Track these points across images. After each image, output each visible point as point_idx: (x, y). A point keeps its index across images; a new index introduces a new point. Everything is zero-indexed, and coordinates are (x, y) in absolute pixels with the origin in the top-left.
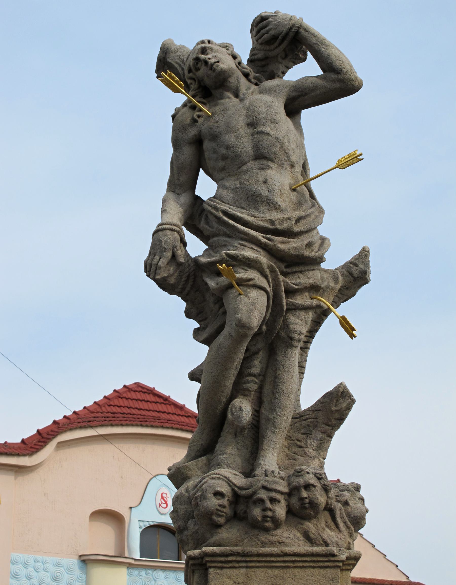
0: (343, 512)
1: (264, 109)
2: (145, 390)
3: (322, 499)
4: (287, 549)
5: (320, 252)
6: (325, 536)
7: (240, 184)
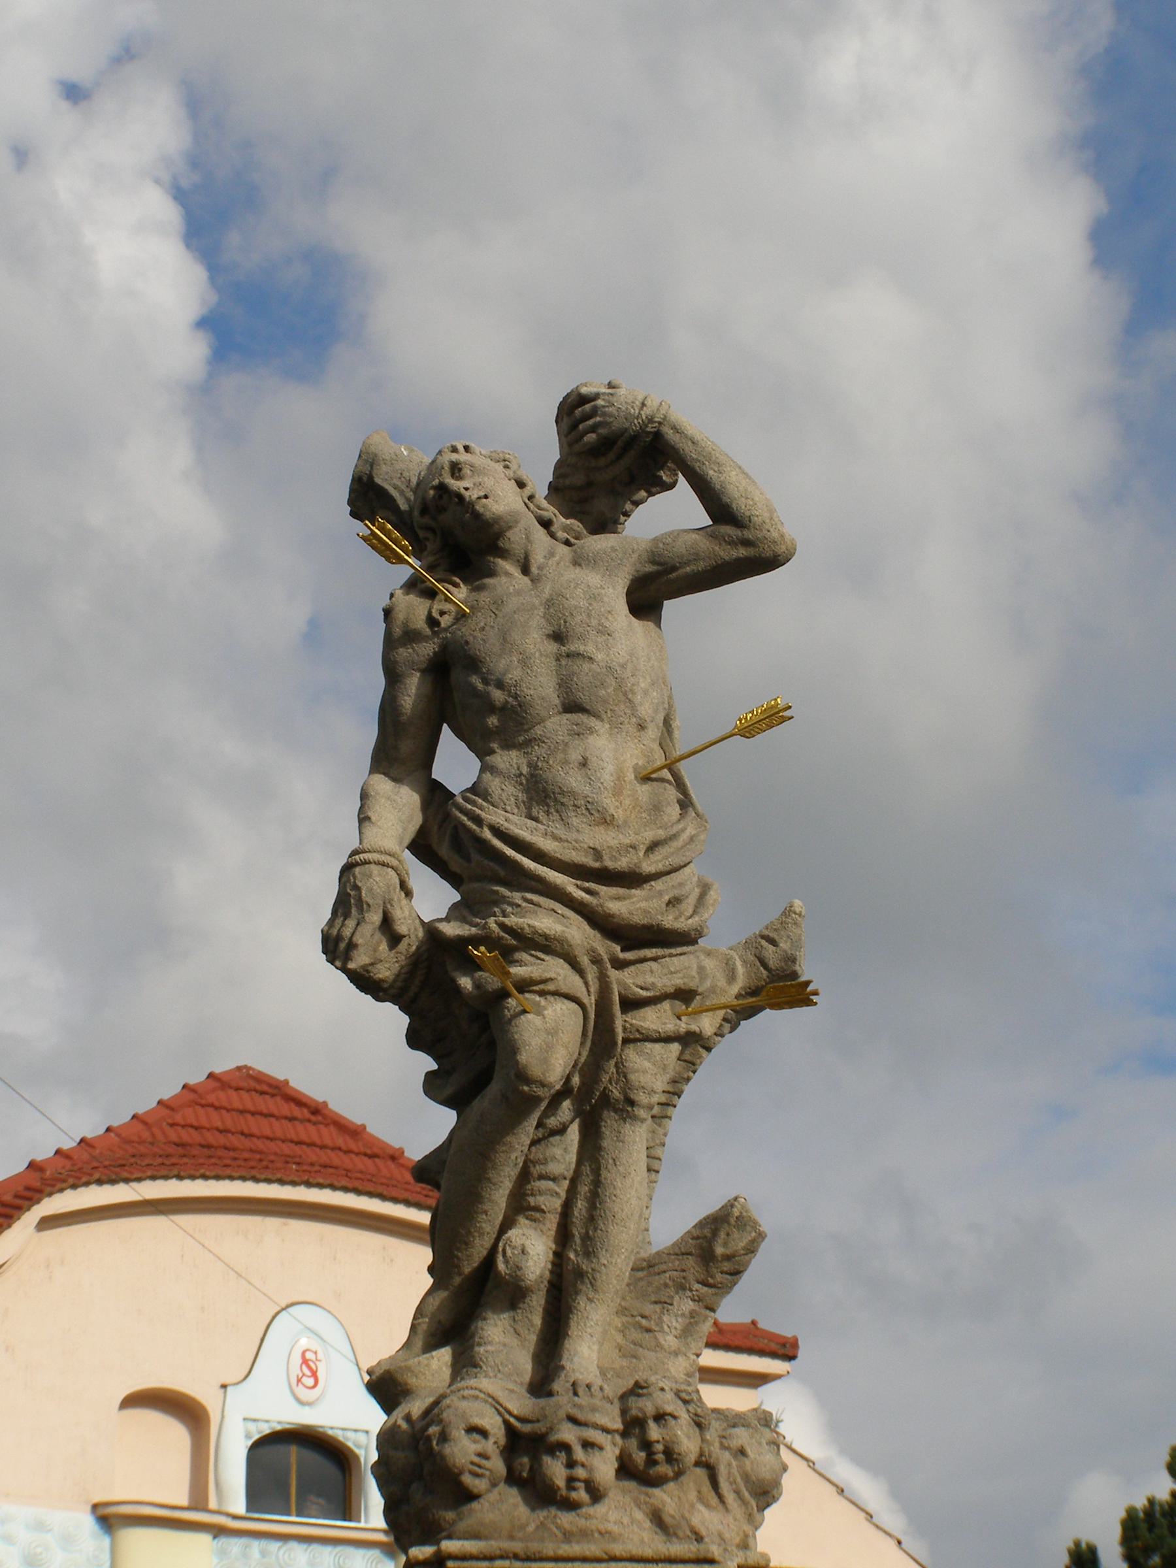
0: (735, 1471)
1: (583, 603)
2: (265, 1088)
3: (688, 1444)
4: (618, 1549)
5: (697, 918)
6: (695, 1521)
7: (530, 765)
